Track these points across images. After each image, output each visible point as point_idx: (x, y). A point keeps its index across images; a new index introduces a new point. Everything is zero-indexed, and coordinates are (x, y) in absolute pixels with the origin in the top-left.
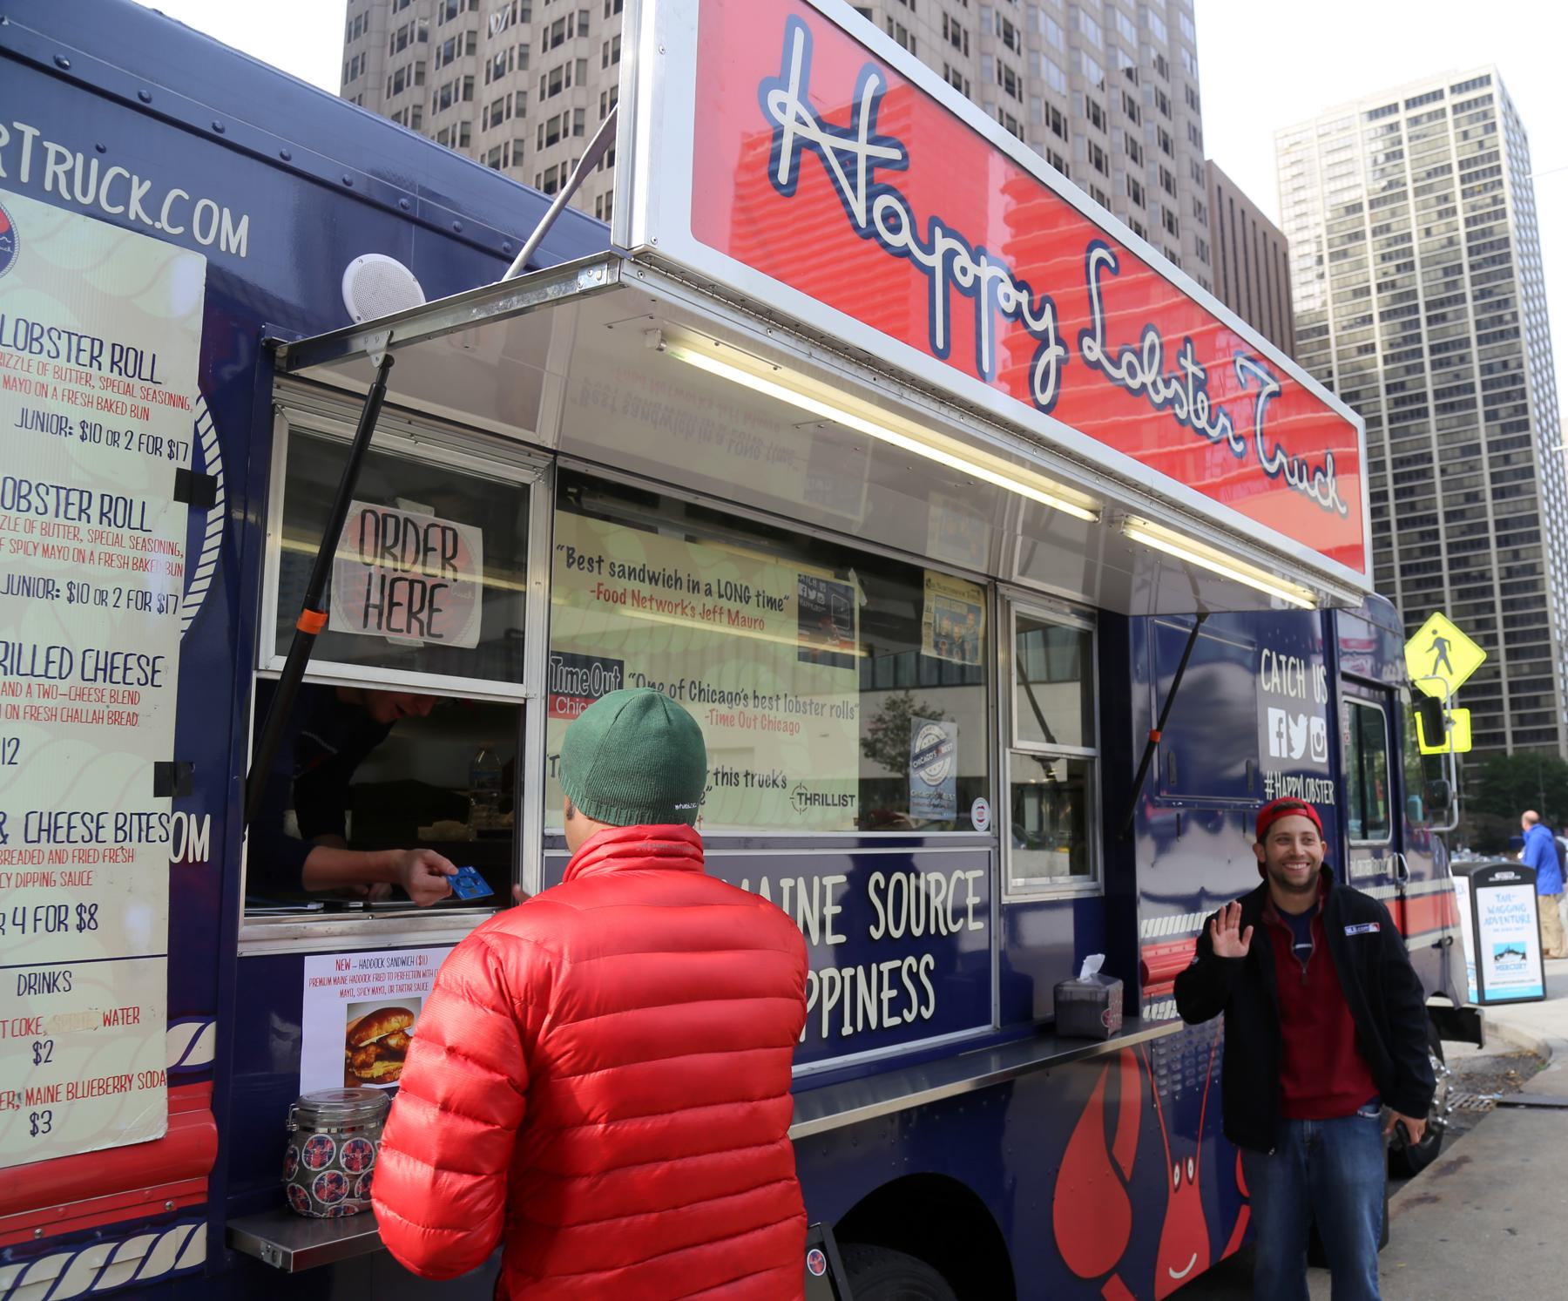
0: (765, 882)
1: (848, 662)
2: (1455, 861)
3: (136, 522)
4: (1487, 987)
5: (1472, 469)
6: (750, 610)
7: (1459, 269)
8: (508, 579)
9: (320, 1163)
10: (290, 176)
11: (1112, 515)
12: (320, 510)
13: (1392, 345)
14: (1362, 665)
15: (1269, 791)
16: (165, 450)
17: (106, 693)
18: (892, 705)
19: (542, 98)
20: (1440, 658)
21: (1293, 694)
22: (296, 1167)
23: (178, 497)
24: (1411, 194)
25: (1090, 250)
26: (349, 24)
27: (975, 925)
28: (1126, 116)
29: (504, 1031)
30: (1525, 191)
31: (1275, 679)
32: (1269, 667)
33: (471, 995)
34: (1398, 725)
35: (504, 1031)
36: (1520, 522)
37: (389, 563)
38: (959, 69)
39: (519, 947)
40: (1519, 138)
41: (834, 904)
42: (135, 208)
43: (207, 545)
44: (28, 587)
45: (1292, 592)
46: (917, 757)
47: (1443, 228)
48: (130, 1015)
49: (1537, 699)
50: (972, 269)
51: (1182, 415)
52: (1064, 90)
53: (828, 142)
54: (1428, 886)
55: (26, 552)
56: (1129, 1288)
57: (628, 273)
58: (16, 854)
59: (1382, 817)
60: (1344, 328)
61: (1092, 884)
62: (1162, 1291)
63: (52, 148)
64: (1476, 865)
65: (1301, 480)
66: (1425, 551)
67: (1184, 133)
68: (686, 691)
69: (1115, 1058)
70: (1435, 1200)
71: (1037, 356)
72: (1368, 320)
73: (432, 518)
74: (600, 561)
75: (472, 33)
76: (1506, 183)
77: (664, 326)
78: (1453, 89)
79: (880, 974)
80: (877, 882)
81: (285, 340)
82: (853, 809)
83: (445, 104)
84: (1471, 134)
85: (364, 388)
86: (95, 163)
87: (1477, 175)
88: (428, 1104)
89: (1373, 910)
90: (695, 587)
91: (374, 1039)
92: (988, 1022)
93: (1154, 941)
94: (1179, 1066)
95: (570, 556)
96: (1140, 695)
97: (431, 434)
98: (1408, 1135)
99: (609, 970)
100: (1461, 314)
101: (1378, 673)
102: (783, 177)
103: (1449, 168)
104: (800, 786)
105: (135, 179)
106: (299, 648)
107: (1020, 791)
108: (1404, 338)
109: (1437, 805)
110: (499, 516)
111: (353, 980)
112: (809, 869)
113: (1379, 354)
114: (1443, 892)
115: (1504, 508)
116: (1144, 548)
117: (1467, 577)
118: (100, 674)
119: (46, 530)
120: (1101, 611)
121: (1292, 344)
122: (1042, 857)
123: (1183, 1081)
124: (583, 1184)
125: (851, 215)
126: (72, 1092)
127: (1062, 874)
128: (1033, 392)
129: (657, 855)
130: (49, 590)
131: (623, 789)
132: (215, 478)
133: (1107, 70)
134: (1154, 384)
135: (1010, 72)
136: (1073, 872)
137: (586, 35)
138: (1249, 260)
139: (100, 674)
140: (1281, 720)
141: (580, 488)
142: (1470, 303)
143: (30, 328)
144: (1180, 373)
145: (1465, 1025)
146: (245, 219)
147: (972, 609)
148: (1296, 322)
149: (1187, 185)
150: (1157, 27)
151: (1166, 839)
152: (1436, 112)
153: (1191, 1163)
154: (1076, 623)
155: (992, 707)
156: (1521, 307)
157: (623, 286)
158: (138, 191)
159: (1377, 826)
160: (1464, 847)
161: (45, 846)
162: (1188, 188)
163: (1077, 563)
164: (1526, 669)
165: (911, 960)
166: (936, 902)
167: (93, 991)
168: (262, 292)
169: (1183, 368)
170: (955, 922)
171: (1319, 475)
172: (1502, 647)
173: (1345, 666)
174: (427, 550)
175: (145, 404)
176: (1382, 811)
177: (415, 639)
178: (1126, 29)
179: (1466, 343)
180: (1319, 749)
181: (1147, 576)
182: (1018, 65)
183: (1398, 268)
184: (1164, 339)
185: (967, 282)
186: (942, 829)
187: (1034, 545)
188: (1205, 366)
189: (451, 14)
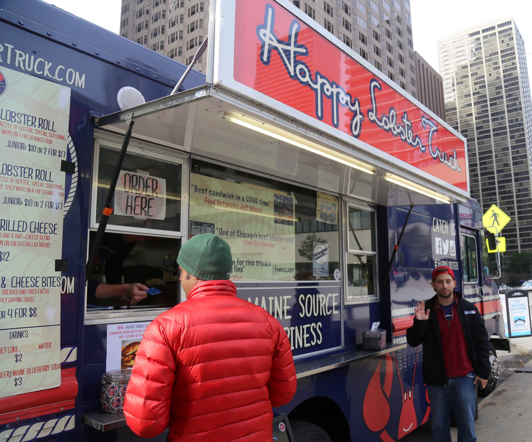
0: (257, 299)
1: (289, 223)
2: (501, 289)
3: (48, 179)
4: (512, 332)
5: (506, 155)
6: (258, 206)
7: (501, 87)
8: (175, 196)
9: (111, 395)
10: (102, 62)
11: (380, 173)
12: (110, 173)
13: (478, 114)
14: (468, 223)
15: (436, 266)
16: (58, 154)
17: (39, 237)
18: (309, 238)
19: (188, 32)
20: (495, 220)
21: (444, 233)
22: (105, 396)
23: (62, 170)
24: (484, 62)
25: (371, 82)
26: (122, 9)
27: (335, 312)
28: (387, 36)
29: (167, 352)
30: (523, 60)
31: (438, 228)
32: (435, 224)
33: (155, 340)
34: (480, 243)
35: (167, 352)
36: (523, 173)
37: (134, 191)
38: (330, 21)
39: (170, 323)
40: (521, 43)
42: (46, 72)
43: (72, 186)
44: (12, 201)
45: (443, 198)
46: (315, 255)
47: (495, 74)
48: (48, 345)
49: (529, 233)
50: (331, 89)
51: (403, 138)
52: (365, 28)
53: (280, 46)
54: (491, 297)
55: (11, 189)
56: (389, 434)
57: (212, 92)
58: (9, 291)
59: (475, 274)
60: (462, 108)
61: (375, 298)
62: (400, 436)
63: (18, 52)
64: (507, 290)
65: (445, 160)
66: (490, 184)
67: (407, 42)
68: (236, 234)
69: (384, 357)
70: (494, 404)
71: (353, 119)
72: (470, 105)
73: (149, 176)
74: (206, 190)
75: (164, 11)
76: (517, 58)
77: (226, 110)
78: (498, 26)
79: (303, 329)
80: (302, 298)
81: (98, 116)
82: (293, 274)
83: (155, 35)
84: (505, 41)
85: (124, 132)
86: (32, 57)
87: (507, 55)
88: (142, 377)
89: (472, 306)
90: (238, 198)
91: (131, 353)
92: (340, 345)
93: (397, 317)
94: (405, 360)
95: (196, 188)
96: (391, 233)
97: (147, 147)
98: (481, 385)
99: (199, 330)
100: (502, 103)
101: (473, 225)
102: (265, 58)
103: (497, 53)
104: (275, 265)
105: (46, 62)
106: (104, 220)
107: (351, 267)
108: (482, 111)
109: (494, 270)
110: (171, 175)
111: (124, 333)
112: (279, 294)
113: (474, 117)
114: (496, 299)
115: (517, 169)
116: (391, 183)
117: (504, 192)
118: (36, 230)
119: (17, 182)
120: (377, 205)
121: (444, 114)
122: (359, 289)
123: (407, 365)
124: (195, 403)
125: (289, 73)
126: (29, 371)
127: (365, 295)
128: (352, 132)
129: (218, 290)
130: (19, 202)
131: (212, 269)
132: (74, 163)
133: (380, 21)
134: (394, 128)
135: (347, 22)
136: (369, 294)
137: (203, 11)
138: (429, 85)
139: (36, 230)
140: (440, 242)
141: (199, 165)
142: (505, 99)
143: (11, 113)
144: (403, 124)
145: (504, 344)
146: (84, 76)
147: (333, 205)
148: (445, 106)
149: (407, 60)
150: (397, 6)
151: (401, 284)
153: (410, 392)
154: (369, 209)
155: (341, 238)
156: (522, 100)
157: (211, 97)
158: (47, 66)
159: (473, 277)
160: (504, 284)
161: (19, 288)
162: (408, 61)
163: (369, 189)
164: (525, 223)
165: (314, 324)
166: (322, 305)
167: (35, 337)
168: (90, 100)
169: (404, 122)
170: (329, 311)
171: (451, 158)
172: (517, 216)
173: (462, 223)
174: (147, 187)
175: (51, 138)
176: (475, 272)
177: (143, 217)
178: (387, 7)
179: (503, 112)
180: (453, 251)
181: (393, 193)
182: (350, 20)
183: (480, 87)
184: (397, 113)
185: (329, 94)
186: (326, 280)
187: (355, 183)
188: (412, 122)
189: (157, 4)
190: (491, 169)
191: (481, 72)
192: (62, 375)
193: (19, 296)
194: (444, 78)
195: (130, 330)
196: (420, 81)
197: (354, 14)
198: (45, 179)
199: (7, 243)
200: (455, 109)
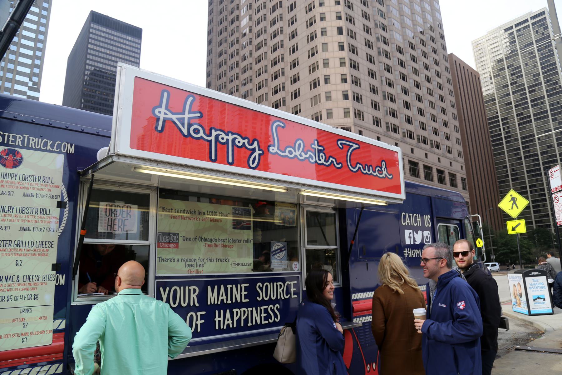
4: (531, 310)
16: (55, 197)
34: (464, 234)
41: (245, 291)
42: (49, 147)
44: (24, 229)
47: (532, 63)
48: (45, 318)
50: (226, 137)
63: (31, 138)
65: (369, 171)
67: (440, 47)
68: (197, 239)
78: (531, 18)
82: (252, 267)
84: (539, 31)
86: (40, 140)
103: (532, 43)
119: (28, 217)
126: (31, 334)
130: (29, 229)
133: (414, 33)
140: (410, 233)
142: (543, 85)
143: (25, 176)
150: (429, 18)
153: (374, 364)
154: (333, 212)
158: (49, 143)
161: (27, 282)
165: (271, 306)
167: (37, 313)
170: (287, 295)
179: (544, 97)
180: (428, 241)
192: (53, 338)
193: (27, 287)
194: (480, 73)
197: (390, 30)
198: (46, 214)
199: (21, 255)
200: (494, 99)
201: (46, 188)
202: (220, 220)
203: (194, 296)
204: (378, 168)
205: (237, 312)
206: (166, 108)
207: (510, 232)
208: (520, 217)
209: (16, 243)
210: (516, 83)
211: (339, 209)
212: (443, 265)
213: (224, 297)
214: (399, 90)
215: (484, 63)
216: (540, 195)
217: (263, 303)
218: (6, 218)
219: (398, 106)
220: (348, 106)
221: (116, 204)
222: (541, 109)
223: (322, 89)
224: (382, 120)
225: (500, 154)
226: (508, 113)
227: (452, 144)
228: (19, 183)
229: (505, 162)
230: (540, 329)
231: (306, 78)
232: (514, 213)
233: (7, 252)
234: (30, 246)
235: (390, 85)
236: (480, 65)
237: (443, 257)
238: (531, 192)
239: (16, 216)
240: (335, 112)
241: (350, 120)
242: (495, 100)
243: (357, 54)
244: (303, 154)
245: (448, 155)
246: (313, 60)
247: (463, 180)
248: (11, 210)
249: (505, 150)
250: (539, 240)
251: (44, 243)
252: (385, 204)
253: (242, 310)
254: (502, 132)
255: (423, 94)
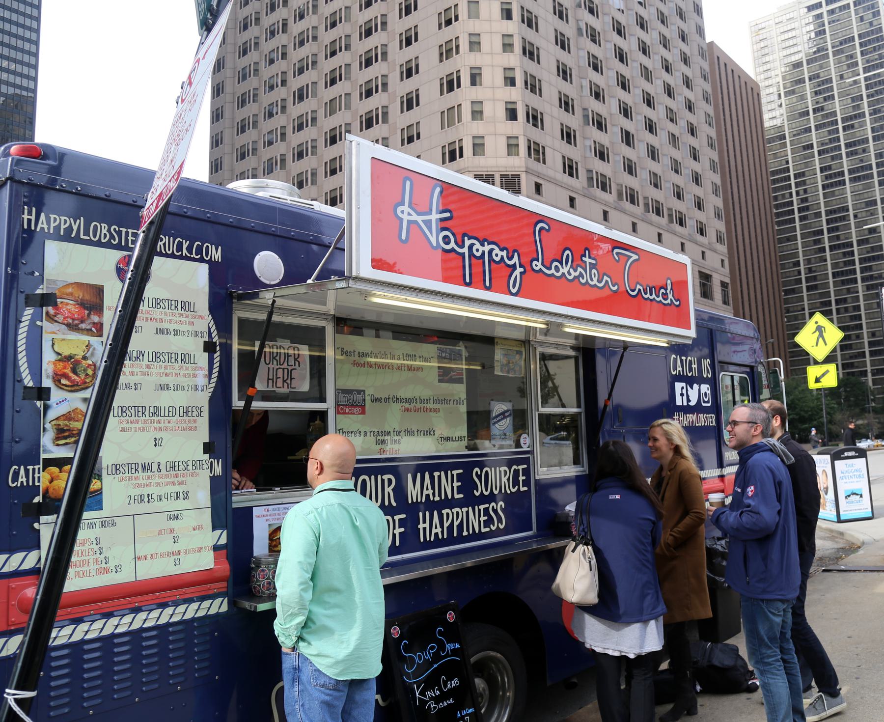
4: (841, 513)
5: (872, 214)
7: (861, 98)
19: (326, 30)
21: (690, 375)
42: (185, 251)
44: (161, 387)
50: (481, 248)
53: (419, 219)
60: (794, 135)
65: (651, 295)
66: (846, 263)
67: (694, 30)
68: (391, 400)
77: (366, 294)
82: (465, 443)
84: (865, 18)
100: (863, 124)
103: (853, 39)
117: (871, 278)
140: (683, 388)
143: (156, 300)
148: (766, 133)
152: (844, 6)
154: (572, 353)
158: (185, 246)
161: (172, 472)
162: (698, 62)
165: (493, 504)
167: (190, 520)
169: (585, 262)
177: (285, 390)
179: (866, 141)
180: (706, 400)
183: (825, 99)
190: (847, 238)
191: (826, 74)
194: (762, 85)
195: (277, 512)
196: (722, 93)
201: (187, 320)
202: (420, 369)
203: (389, 490)
204: (662, 291)
205: (448, 514)
206: (410, 206)
207: (812, 385)
208: (829, 360)
209: (152, 410)
210: (822, 109)
211: (583, 348)
212: (756, 433)
213: (430, 492)
214: (615, 109)
215: (768, 66)
216: (853, 318)
217: (483, 499)
218: (135, 370)
219: (610, 138)
220: (515, 133)
221: (278, 344)
222: (862, 161)
223: (465, 94)
224: (579, 164)
225: (788, 239)
226: (806, 165)
227: (707, 216)
228: (148, 312)
229: (796, 255)
230: (854, 541)
231: (432, 71)
232: (819, 352)
233: (140, 425)
234: (171, 414)
235: (597, 96)
236: (761, 69)
237: (758, 422)
238: (838, 310)
239: (148, 367)
240: (489, 143)
241: (518, 163)
242: (785, 138)
243: (537, 31)
244: (572, 271)
245: (699, 237)
246: (448, 33)
247: (724, 285)
248: (141, 357)
249: (798, 233)
250: (847, 399)
251: (190, 409)
252: (666, 345)
253: (455, 510)
254: (795, 198)
255: (659, 119)
